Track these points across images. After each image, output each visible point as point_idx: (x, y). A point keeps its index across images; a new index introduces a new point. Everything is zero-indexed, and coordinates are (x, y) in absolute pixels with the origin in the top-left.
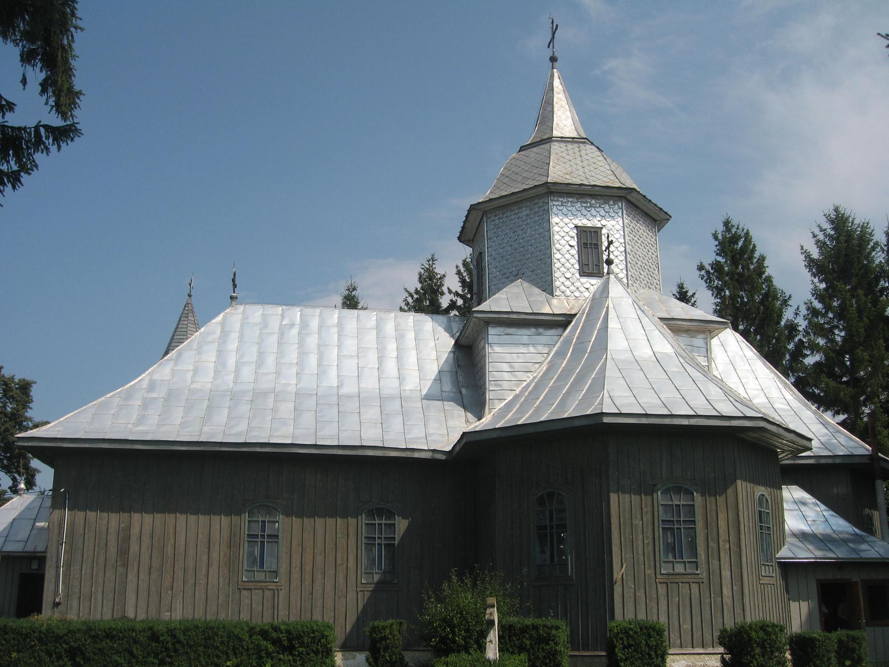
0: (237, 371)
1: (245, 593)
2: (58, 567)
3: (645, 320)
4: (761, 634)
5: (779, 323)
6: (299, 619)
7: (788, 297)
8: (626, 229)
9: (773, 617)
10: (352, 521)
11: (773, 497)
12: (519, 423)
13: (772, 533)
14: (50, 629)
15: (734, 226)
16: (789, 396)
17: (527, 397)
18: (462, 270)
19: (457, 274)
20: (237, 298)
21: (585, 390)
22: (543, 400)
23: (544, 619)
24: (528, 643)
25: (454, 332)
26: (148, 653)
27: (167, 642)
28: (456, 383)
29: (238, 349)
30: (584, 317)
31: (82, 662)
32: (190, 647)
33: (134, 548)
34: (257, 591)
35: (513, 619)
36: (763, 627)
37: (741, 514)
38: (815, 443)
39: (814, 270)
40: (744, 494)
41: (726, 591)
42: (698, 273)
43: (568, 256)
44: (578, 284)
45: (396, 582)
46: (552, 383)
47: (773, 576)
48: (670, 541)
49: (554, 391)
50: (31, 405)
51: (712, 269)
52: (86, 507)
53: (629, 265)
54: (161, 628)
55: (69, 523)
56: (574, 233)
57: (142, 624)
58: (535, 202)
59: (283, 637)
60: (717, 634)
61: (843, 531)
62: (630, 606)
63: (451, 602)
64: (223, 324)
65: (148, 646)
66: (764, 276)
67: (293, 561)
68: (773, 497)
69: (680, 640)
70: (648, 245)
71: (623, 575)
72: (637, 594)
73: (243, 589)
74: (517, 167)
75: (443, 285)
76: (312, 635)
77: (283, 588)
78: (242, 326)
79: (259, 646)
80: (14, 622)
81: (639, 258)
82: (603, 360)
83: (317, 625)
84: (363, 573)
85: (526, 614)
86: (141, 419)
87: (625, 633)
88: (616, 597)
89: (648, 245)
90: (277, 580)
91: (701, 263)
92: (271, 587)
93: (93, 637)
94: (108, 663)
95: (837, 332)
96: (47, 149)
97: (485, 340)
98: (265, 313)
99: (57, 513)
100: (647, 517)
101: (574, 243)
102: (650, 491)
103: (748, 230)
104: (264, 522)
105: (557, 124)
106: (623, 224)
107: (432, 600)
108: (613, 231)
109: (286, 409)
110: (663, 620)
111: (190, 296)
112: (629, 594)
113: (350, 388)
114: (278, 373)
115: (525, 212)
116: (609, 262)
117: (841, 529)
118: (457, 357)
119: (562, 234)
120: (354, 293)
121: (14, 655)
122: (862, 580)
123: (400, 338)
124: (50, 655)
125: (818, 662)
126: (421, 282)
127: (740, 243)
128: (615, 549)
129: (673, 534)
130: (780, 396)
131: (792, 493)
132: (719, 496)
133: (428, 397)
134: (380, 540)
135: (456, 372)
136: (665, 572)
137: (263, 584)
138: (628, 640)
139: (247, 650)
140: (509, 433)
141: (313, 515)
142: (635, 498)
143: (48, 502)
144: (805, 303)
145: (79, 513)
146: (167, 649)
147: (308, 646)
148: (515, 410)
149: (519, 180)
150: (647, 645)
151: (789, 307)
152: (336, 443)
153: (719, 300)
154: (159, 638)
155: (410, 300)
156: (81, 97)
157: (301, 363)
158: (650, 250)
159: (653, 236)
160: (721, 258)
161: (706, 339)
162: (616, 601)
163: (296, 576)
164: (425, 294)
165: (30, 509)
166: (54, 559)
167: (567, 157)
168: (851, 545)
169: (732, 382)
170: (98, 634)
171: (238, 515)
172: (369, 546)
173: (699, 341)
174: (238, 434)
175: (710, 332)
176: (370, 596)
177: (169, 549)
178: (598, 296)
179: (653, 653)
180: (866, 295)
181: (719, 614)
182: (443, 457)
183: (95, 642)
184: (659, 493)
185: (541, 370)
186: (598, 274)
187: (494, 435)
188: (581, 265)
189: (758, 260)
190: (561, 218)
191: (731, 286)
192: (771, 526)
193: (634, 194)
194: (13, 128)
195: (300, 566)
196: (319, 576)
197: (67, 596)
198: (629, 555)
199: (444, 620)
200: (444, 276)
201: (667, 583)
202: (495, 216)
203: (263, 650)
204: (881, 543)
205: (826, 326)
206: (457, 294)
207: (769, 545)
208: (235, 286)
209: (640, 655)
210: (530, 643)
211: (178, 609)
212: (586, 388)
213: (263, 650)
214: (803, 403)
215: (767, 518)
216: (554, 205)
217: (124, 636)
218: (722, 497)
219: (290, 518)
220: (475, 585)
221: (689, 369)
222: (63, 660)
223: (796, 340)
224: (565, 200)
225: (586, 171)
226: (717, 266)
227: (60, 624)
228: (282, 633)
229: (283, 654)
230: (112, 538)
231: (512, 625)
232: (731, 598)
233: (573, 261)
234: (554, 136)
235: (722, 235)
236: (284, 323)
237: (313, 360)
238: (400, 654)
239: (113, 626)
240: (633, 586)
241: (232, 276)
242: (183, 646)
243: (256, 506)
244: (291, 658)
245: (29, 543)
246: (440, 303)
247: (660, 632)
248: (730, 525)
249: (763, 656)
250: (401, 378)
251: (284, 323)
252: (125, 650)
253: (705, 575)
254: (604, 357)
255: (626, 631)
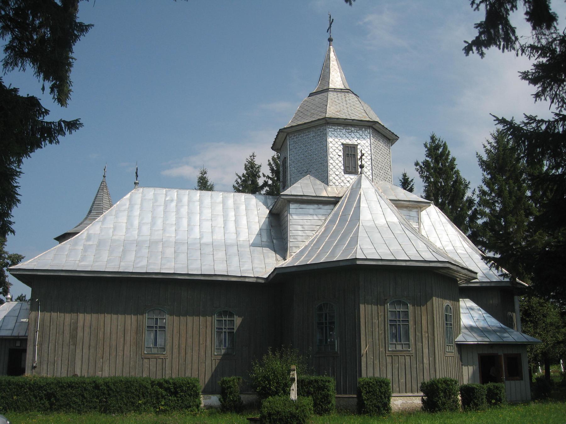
0: (140, 228)
1: (146, 361)
2: (34, 346)
3: (382, 202)
4: (444, 385)
5: (463, 198)
6: (177, 376)
7: (468, 183)
8: (372, 145)
9: (451, 375)
10: (209, 318)
11: (454, 306)
12: (308, 263)
13: (453, 327)
14: (36, 382)
15: (437, 139)
16: (466, 246)
17: (312, 247)
18: (272, 162)
19: (268, 165)
20: (138, 184)
21: (346, 244)
22: (322, 249)
23: (321, 376)
24: (312, 390)
25: (269, 205)
26: (93, 396)
27: (104, 390)
28: (270, 237)
29: (140, 215)
30: (346, 200)
31: (54, 402)
32: (118, 392)
33: (80, 334)
34: (153, 359)
35: (303, 377)
36: (445, 381)
37: (435, 317)
38: (480, 275)
39: (484, 167)
40: (437, 304)
41: (426, 361)
42: (415, 167)
43: (337, 162)
44: (343, 178)
45: (234, 354)
46: (327, 239)
47: (453, 352)
48: (394, 332)
49: (329, 244)
50: (6, 243)
51: (423, 165)
52: (52, 310)
53: (373, 167)
54: (101, 381)
55: (41, 319)
56: (341, 148)
57: (89, 379)
58: (318, 128)
59: (171, 387)
60: (419, 385)
61: (494, 326)
62: (370, 369)
63: (268, 366)
64: (130, 199)
65: (93, 392)
66: (454, 170)
67: (174, 341)
68: (454, 306)
69: (398, 389)
70: (385, 154)
71: (367, 351)
72: (375, 362)
73: (145, 358)
74: (307, 107)
75: (260, 172)
76: (188, 385)
77: (168, 357)
78: (142, 200)
79: (157, 391)
80: (14, 378)
81: (380, 163)
82: (357, 226)
83: (191, 380)
84: (215, 349)
85: (311, 373)
86: (83, 258)
87: (368, 384)
88: (362, 364)
89: (385, 154)
90: (165, 353)
91: (417, 161)
92: (161, 357)
93: (61, 387)
94: (70, 402)
95: (497, 205)
96: (65, 134)
97: (288, 211)
98: (155, 193)
99: (33, 314)
100: (381, 319)
101: (341, 154)
102: (383, 303)
103: (445, 142)
104: (157, 319)
105: (332, 80)
106: (370, 143)
107: (257, 365)
108: (364, 147)
109: (170, 252)
110: (389, 377)
111: (104, 177)
112: (370, 362)
113: (207, 239)
114: (164, 230)
115: (312, 134)
116: (362, 167)
117: (493, 324)
118: (271, 221)
119: (334, 148)
120: (205, 175)
121: (15, 397)
122: (505, 355)
123: (236, 209)
124: (36, 398)
125: (476, 401)
126: (246, 170)
127: (441, 150)
128: (363, 336)
129: (396, 328)
130: (461, 245)
131: (466, 304)
132: (423, 306)
133: (254, 245)
134: (225, 330)
135: (270, 230)
136: (391, 350)
137: (156, 355)
138: (369, 388)
139: (150, 394)
140: (304, 269)
141: (186, 314)
142: (375, 307)
143: (27, 306)
144: (478, 187)
145: (47, 313)
146: (104, 394)
147: (186, 392)
148: (305, 255)
149: (309, 114)
150: (380, 391)
151: (468, 189)
152: (200, 273)
153: (427, 184)
154: (99, 388)
155: (239, 181)
156: (71, 93)
157: (178, 224)
158: (386, 157)
159: (388, 149)
160: (429, 158)
161: (418, 212)
162: (362, 366)
163: (175, 350)
164: (248, 177)
165: (14, 310)
166: (32, 341)
167: (338, 101)
168: (498, 334)
169: (433, 238)
170: (64, 385)
171: (141, 315)
172: (219, 333)
173: (413, 213)
174: (142, 267)
175: (421, 208)
176: (219, 363)
177: (101, 335)
178: (354, 187)
179: (383, 396)
180: (514, 183)
181: (421, 373)
182: (263, 281)
183: (62, 390)
184: (388, 304)
185: (321, 231)
186: (355, 172)
187: (293, 270)
188: (345, 167)
189: (451, 160)
190: (333, 138)
191: (434, 176)
192: (452, 323)
193: (377, 125)
194: (47, 122)
195: (178, 344)
196: (189, 351)
197: (40, 362)
198: (371, 340)
199: (264, 377)
200: (260, 166)
201: (392, 356)
202: (294, 136)
203: (159, 394)
204: (515, 333)
205: (490, 201)
206: (268, 177)
207: (451, 333)
208: (137, 176)
209: (376, 397)
210: (314, 390)
211: (106, 370)
212: (347, 243)
213: (159, 394)
214: (474, 250)
215: (450, 319)
216: (329, 131)
217: (79, 387)
218: (424, 307)
219: (172, 317)
220: (281, 357)
221: (407, 232)
222: (43, 401)
223: (473, 209)
224: (336, 128)
225: (349, 110)
226: (426, 163)
227: (41, 380)
228: (170, 384)
229: (171, 397)
230: (67, 328)
231: (303, 380)
232: (428, 364)
233: (340, 165)
234: (330, 88)
235: (430, 145)
236: (167, 199)
237: (185, 222)
238: (238, 396)
239: (73, 381)
240: (373, 358)
241: (136, 171)
242: (113, 392)
243: (152, 310)
244: (176, 398)
245: (15, 331)
246: (258, 183)
247: (387, 384)
248: (428, 323)
249: (445, 398)
250: (237, 233)
251: (167, 199)
252: (80, 394)
253: (414, 351)
254: (358, 224)
255: (368, 384)
